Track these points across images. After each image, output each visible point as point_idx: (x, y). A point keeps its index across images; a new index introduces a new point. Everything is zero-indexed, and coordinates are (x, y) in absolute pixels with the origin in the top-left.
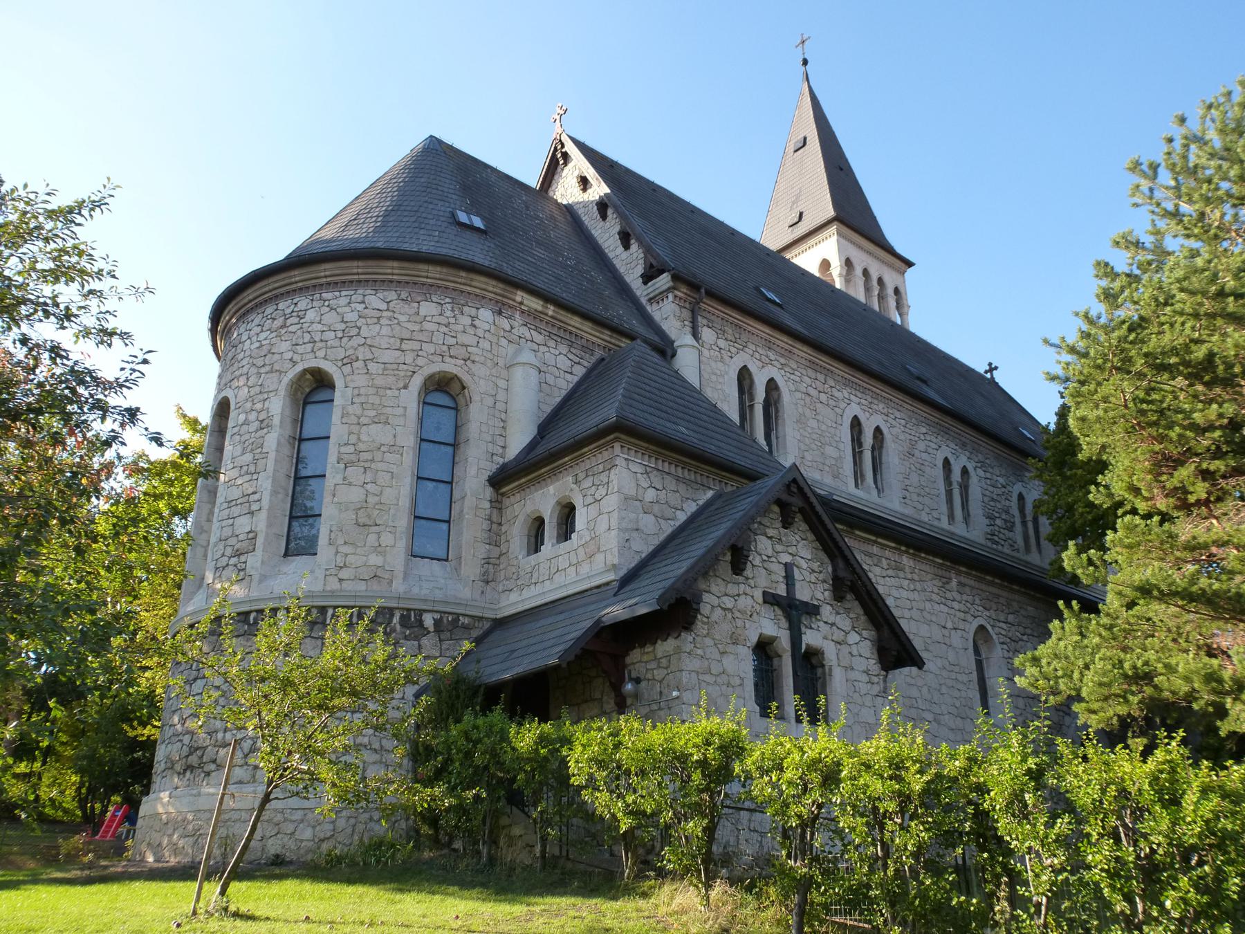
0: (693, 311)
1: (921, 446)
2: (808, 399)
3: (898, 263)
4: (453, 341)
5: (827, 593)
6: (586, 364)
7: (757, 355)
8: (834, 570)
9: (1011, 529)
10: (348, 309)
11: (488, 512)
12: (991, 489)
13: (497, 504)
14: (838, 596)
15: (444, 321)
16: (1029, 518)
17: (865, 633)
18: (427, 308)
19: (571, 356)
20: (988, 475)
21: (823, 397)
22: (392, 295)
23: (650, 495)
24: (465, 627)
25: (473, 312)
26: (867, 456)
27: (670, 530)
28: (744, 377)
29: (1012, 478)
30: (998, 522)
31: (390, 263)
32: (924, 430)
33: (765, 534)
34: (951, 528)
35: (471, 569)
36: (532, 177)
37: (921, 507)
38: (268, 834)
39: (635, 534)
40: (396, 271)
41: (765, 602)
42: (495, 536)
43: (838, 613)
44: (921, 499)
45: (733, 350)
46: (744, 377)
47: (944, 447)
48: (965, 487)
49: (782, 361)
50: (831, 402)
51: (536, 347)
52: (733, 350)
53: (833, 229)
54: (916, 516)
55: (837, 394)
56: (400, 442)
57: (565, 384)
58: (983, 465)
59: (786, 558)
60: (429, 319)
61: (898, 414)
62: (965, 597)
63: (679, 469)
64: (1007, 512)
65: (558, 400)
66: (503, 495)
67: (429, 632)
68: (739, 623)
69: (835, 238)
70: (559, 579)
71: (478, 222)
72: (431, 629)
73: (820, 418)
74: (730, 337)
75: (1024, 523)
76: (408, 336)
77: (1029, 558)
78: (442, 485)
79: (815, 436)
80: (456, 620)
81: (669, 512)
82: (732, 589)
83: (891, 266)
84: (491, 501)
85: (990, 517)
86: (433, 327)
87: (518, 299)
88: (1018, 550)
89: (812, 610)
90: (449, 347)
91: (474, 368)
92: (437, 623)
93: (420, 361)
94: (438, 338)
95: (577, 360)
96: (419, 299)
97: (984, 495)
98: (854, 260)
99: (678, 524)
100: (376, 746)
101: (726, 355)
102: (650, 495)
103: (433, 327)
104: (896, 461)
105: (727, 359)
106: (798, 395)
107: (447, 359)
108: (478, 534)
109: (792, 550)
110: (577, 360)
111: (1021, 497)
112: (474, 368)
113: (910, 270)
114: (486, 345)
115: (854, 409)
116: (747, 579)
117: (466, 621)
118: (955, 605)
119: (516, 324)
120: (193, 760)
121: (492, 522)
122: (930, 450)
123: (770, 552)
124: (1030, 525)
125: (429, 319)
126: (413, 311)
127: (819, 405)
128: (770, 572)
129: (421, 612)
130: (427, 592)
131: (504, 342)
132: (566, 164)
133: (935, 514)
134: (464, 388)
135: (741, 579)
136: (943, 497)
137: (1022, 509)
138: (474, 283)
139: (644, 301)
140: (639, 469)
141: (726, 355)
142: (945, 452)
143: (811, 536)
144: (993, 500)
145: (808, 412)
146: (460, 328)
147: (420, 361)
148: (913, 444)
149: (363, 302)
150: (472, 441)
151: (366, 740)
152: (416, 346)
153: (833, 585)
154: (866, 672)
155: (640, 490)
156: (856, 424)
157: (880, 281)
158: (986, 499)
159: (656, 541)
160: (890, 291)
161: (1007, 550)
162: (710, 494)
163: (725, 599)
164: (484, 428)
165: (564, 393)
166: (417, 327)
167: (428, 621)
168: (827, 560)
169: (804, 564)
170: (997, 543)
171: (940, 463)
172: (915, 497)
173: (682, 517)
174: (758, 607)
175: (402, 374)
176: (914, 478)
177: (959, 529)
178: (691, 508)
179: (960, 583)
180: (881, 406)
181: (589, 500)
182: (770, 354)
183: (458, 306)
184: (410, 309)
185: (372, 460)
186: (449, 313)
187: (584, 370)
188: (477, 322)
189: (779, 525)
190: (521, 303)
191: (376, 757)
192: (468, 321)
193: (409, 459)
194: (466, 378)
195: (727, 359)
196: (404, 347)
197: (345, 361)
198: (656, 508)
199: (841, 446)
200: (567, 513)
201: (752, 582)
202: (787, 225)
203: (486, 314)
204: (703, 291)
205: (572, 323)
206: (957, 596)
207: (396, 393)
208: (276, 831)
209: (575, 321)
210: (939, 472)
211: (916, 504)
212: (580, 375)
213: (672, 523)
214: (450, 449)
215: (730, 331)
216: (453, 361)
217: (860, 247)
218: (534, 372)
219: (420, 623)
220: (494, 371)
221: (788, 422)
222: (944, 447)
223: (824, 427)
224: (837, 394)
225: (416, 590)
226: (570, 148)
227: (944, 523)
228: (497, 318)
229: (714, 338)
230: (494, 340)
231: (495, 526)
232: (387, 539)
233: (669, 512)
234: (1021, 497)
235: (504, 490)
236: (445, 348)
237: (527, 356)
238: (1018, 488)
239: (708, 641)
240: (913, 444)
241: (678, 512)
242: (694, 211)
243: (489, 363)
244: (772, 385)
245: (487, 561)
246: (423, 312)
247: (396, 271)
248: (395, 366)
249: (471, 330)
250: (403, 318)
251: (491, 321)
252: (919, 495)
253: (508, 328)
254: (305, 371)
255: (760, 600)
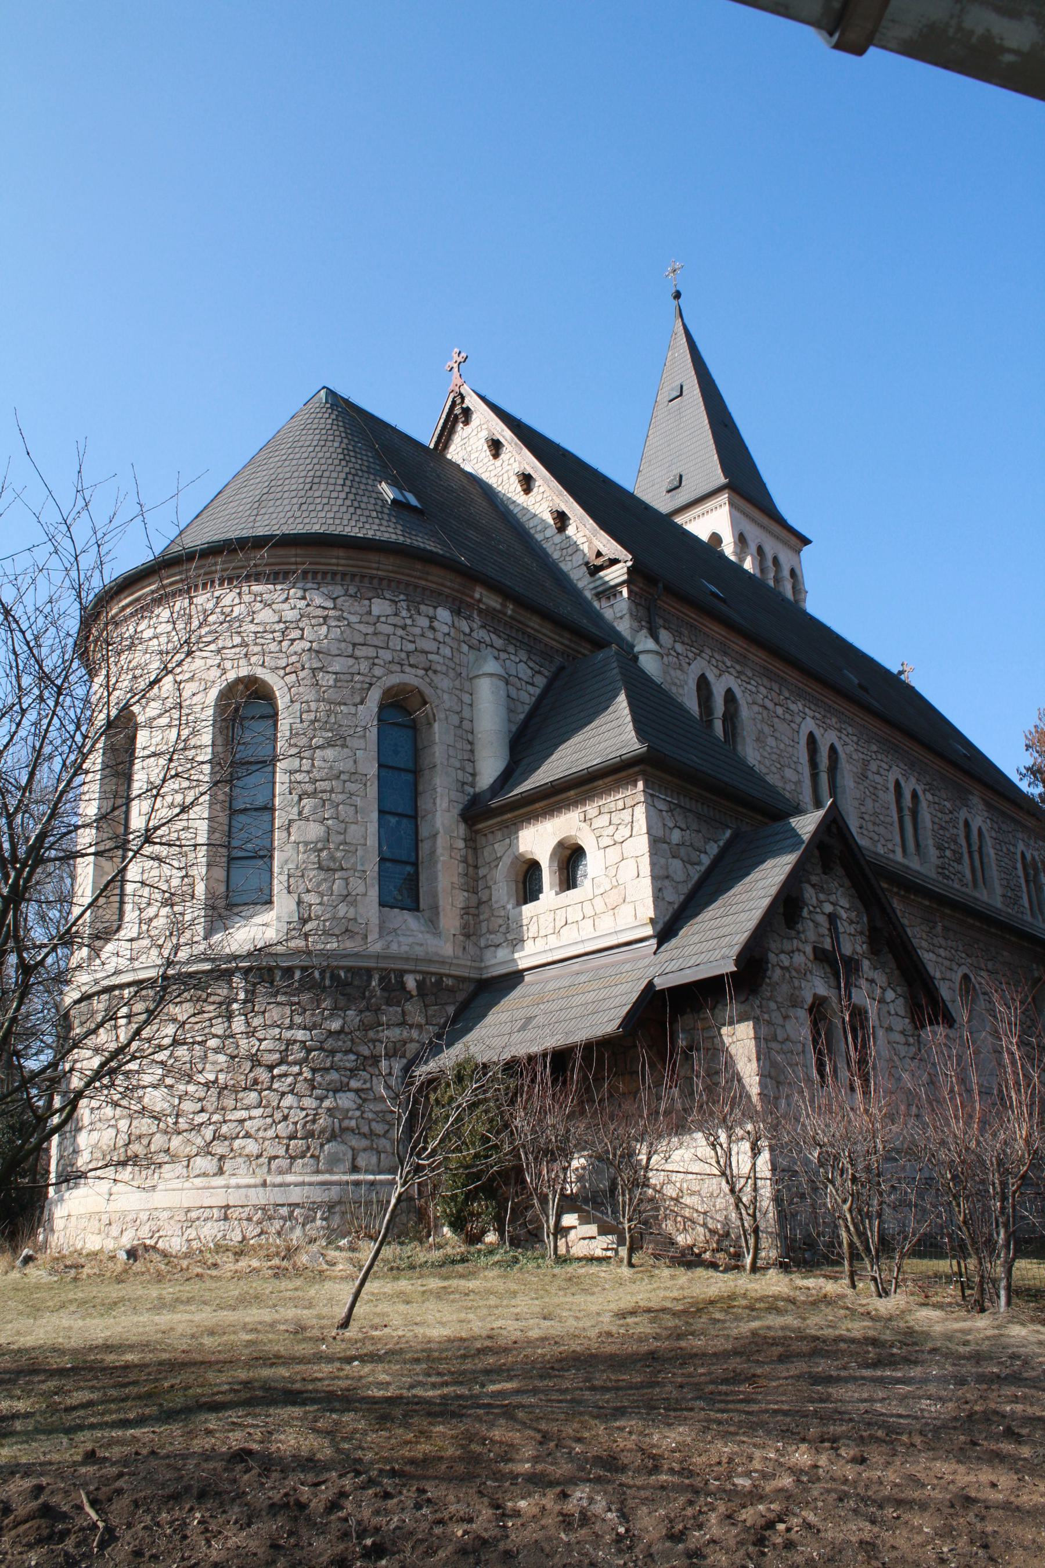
0: (648, 609)
1: (873, 766)
2: (765, 713)
3: (793, 540)
4: (411, 647)
5: (865, 946)
6: (547, 673)
7: (714, 662)
8: (870, 920)
9: (959, 861)
10: (286, 606)
11: (463, 852)
12: (939, 815)
13: (473, 842)
14: (874, 950)
15: (400, 622)
16: (975, 847)
17: (898, 989)
18: (380, 607)
19: (531, 664)
20: (937, 799)
21: (780, 710)
22: (338, 590)
23: (676, 836)
24: (451, 990)
25: (431, 611)
26: (824, 778)
27: (696, 877)
28: (703, 685)
29: (958, 803)
30: (948, 853)
31: (336, 552)
32: (874, 748)
33: (809, 882)
34: (906, 862)
35: (450, 921)
36: (428, 438)
37: (876, 838)
38: (248, 1235)
39: (667, 883)
40: (342, 562)
41: (816, 958)
42: (474, 881)
43: (875, 969)
44: (876, 829)
45: (691, 655)
46: (703, 685)
47: (894, 768)
48: (915, 813)
49: (738, 667)
50: (788, 716)
51: (496, 653)
52: (691, 655)
53: (724, 497)
54: (872, 848)
55: (793, 707)
56: (362, 769)
57: (528, 697)
58: (930, 788)
59: (828, 908)
60: (383, 619)
61: (850, 730)
62: (949, 943)
63: (699, 805)
64: (955, 842)
65: (522, 716)
66: (477, 832)
67: (412, 997)
68: (796, 983)
69: (726, 508)
70: (569, 935)
71: (413, 501)
72: (415, 993)
73: (777, 735)
74: (686, 640)
75: (970, 853)
76: (361, 640)
77: (976, 894)
78: (405, 821)
79: (774, 757)
80: (440, 981)
81: (694, 856)
82: (787, 946)
83: (785, 543)
84: (465, 840)
85: (940, 848)
86: (389, 629)
87: (477, 596)
88: (967, 885)
89: (852, 966)
90: (408, 653)
91: (437, 679)
92: (420, 985)
93: (378, 671)
94: (395, 643)
95: (537, 668)
96: (370, 595)
97: (933, 822)
98: (749, 537)
99: (703, 868)
100: (365, 1129)
101: (684, 661)
102: (676, 836)
103: (389, 629)
104: (852, 785)
105: (685, 666)
106: (756, 708)
107: (407, 669)
108: (455, 879)
109: (833, 898)
110: (537, 668)
111: (967, 824)
112: (437, 679)
113: (805, 548)
114: (447, 651)
115: (809, 725)
116: (798, 933)
117: (450, 982)
118: (942, 952)
119: (475, 626)
120: (136, 1148)
121: (468, 865)
122: (882, 772)
123: (814, 901)
124: (976, 856)
125: (383, 619)
126: (365, 609)
127: (776, 720)
128: (817, 925)
129: (402, 973)
130: (407, 948)
131: (465, 648)
132: (466, 423)
133: (890, 846)
134: (425, 703)
135: (793, 933)
136: (896, 825)
137: (968, 837)
138: (430, 578)
139: (588, 594)
140: (663, 806)
141: (684, 661)
142: (895, 774)
143: (847, 883)
144: (942, 828)
145: (767, 730)
146: (417, 631)
147: (378, 671)
148: (866, 764)
149: (304, 598)
150: (439, 767)
151: (353, 1123)
152: (371, 652)
153: (869, 937)
154: (902, 1032)
155: (667, 831)
156: (812, 739)
157: (776, 561)
158: (936, 827)
159: (685, 889)
160: (786, 573)
161: (957, 886)
162: (728, 833)
163: (782, 956)
164: (452, 752)
165: (527, 708)
166: (370, 630)
167: (411, 982)
168: (862, 909)
169: (844, 916)
170: (948, 878)
171: (891, 786)
172: (870, 827)
173: (706, 860)
174: (809, 964)
175: (358, 686)
176: (869, 802)
177: (915, 864)
178: (713, 849)
179: (944, 927)
180: (834, 720)
181: (606, 841)
182: (726, 659)
183: (414, 605)
184: (360, 607)
185: (332, 791)
186: (404, 613)
187: (545, 680)
188: (436, 624)
189: (819, 871)
190: (480, 601)
191: (365, 1143)
192: (424, 622)
193: (373, 791)
194: (428, 691)
195: (685, 666)
196: (358, 653)
197: (288, 670)
198: (683, 851)
199: (800, 769)
200: (570, 859)
201: (803, 936)
202: (664, 489)
203: (443, 614)
204: (661, 585)
205: (532, 624)
206: (943, 942)
207: (353, 710)
208: (258, 1230)
209: (534, 623)
210: (891, 797)
211: (872, 834)
212: (542, 686)
213: (698, 868)
214: (410, 777)
215: (686, 633)
216: (413, 671)
217: (753, 520)
218: (502, 684)
219: (402, 985)
220: (457, 683)
221: (748, 740)
222: (894, 768)
223: (782, 746)
224: (793, 707)
225: (394, 948)
226: (472, 401)
227: (899, 857)
228: (456, 620)
229: (671, 641)
230: (455, 645)
231: (471, 869)
232: (357, 886)
233: (694, 856)
234: (967, 824)
235: (480, 826)
236: (403, 655)
237: (491, 666)
238: (963, 814)
239: (773, 1005)
240: (866, 764)
241: (703, 856)
242: (394, 430)
243: (452, 674)
244: (730, 697)
245: (466, 911)
246: (376, 611)
247: (342, 562)
248: (349, 677)
249: (430, 634)
250: (354, 619)
251: (450, 623)
252: (874, 824)
253: (467, 630)
254: (239, 680)
255: (811, 957)
